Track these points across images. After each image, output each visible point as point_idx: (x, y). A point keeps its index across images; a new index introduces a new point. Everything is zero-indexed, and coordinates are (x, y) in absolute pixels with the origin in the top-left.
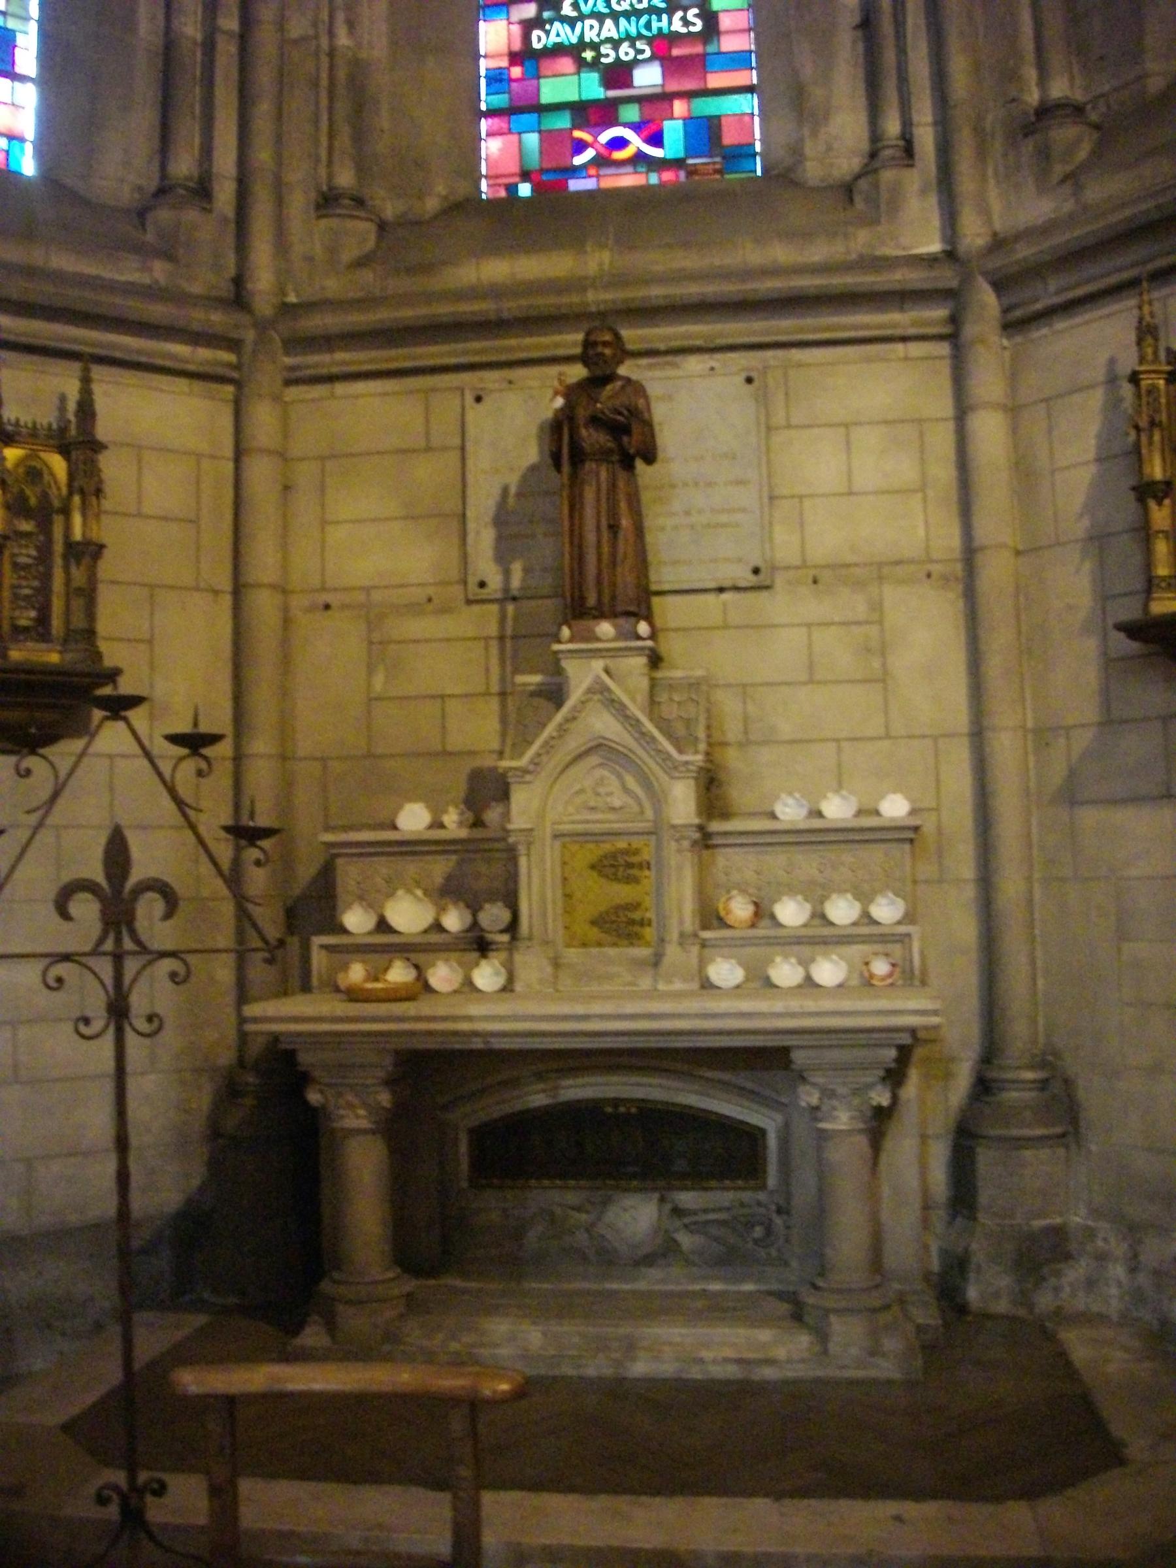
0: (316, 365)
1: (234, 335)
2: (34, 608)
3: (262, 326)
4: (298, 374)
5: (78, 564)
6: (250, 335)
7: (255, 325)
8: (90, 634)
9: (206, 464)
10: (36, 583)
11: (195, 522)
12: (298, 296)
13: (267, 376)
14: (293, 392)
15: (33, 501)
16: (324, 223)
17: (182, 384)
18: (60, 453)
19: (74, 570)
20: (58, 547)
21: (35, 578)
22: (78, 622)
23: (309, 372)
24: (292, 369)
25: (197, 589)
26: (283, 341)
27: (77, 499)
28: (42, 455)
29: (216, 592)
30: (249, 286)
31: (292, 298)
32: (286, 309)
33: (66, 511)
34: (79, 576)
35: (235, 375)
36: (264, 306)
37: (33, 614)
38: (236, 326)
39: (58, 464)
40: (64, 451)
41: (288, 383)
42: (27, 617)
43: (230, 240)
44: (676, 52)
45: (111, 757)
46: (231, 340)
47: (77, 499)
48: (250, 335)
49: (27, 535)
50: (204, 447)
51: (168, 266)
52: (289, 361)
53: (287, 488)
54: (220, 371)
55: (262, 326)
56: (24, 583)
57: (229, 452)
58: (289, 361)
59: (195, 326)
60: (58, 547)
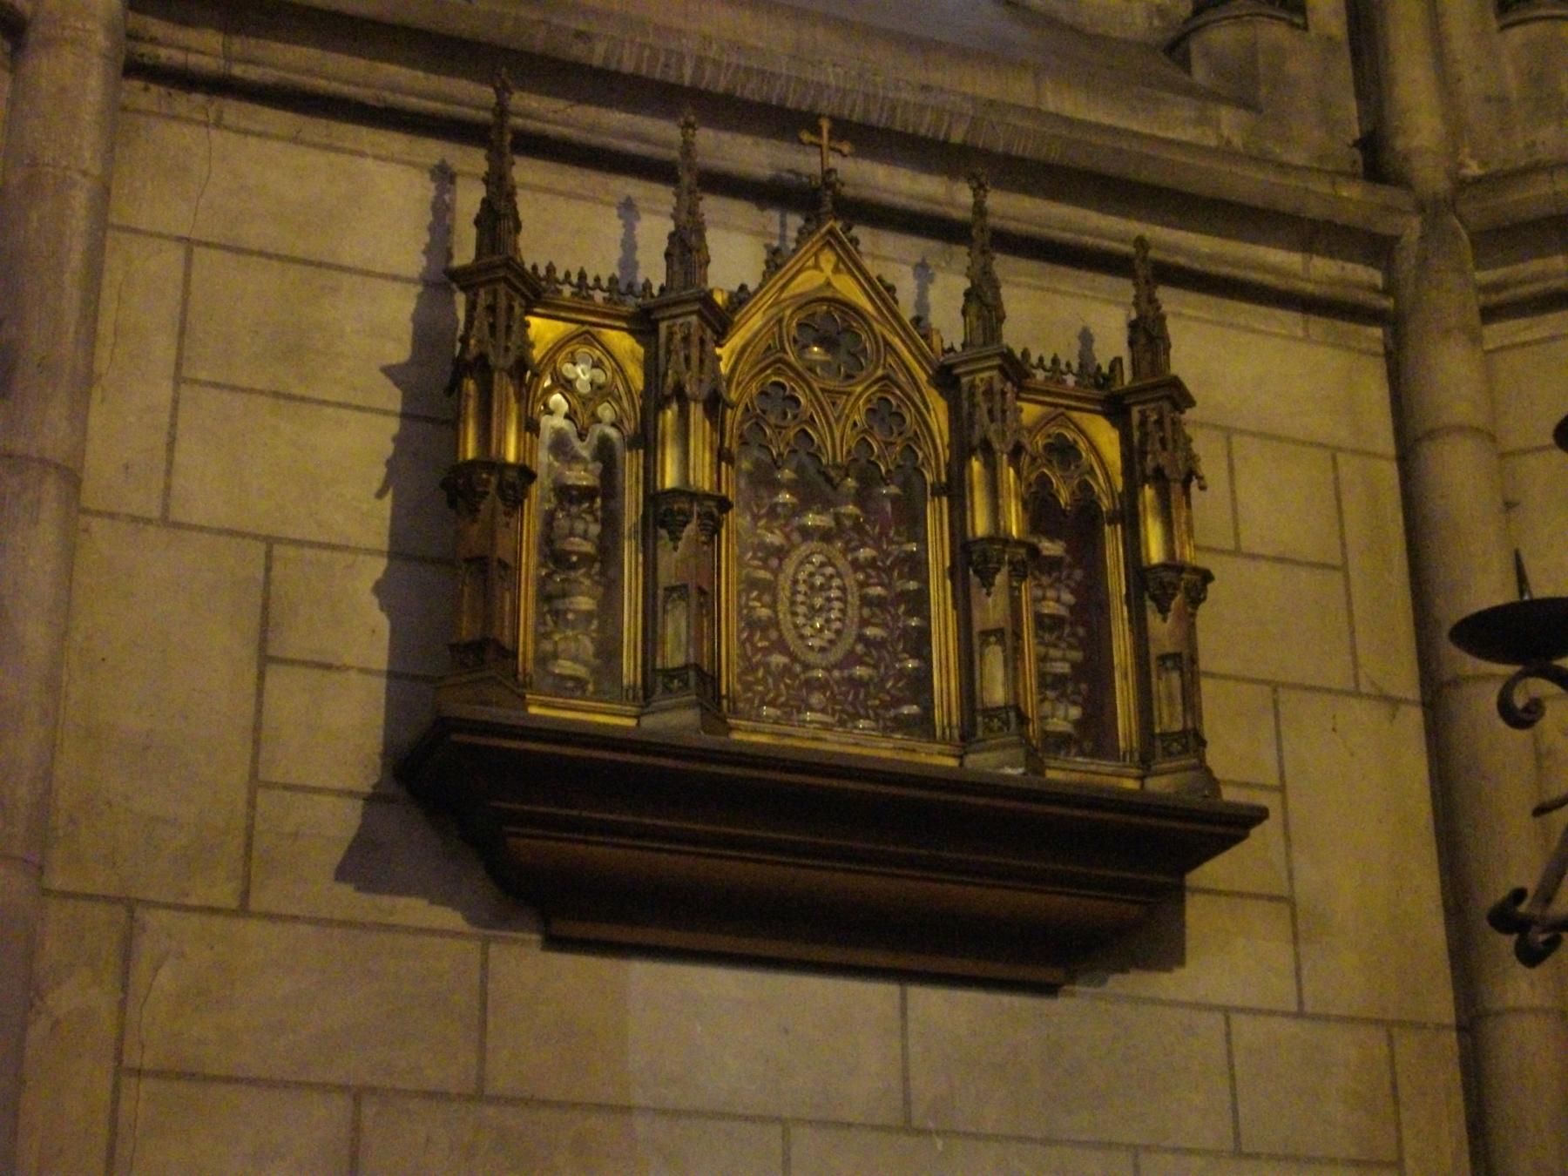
0: (1542, 276)
1: (1383, 227)
2: (1074, 703)
3: (1431, 210)
4: (1504, 296)
5: (1163, 610)
6: (1411, 229)
7: (1420, 208)
8: (1193, 740)
9: (1349, 467)
10: (1076, 655)
11: (1344, 568)
12: (1483, 164)
13: (1451, 292)
14: (1496, 333)
15: (1064, 497)
16: (1517, 35)
17: (1288, 321)
18: (1107, 415)
19: (1154, 620)
20: (1117, 583)
21: (1071, 647)
22: (1169, 719)
23: (1525, 290)
24: (1497, 287)
25: (1357, 694)
26: (1471, 234)
27: (1149, 493)
28: (1075, 415)
29: (1393, 702)
30: (1400, 144)
31: (1473, 169)
32: (1462, 185)
33: (1130, 521)
34: (1162, 629)
35: (1388, 303)
36: (1431, 176)
37: (1075, 712)
38: (1388, 209)
39: (1106, 438)
40: (1115, 409)
41: (1490, 314)
42: (1064, 717)
43: (1343, 70)
44: (470, 386)
45: (1227, 1011)
46: (1373, 238)
47: (1149, 493)
48: (1411, 229)
49: (1053, 564)
50: (1342, 435)
51: (1243, 114)
52: (1483, 277)
53: (1509, 505)
54: (1362, 296)
55: (1431, 210)
56: (1053, 653)
57: (1385, 442)
58: (1483, 277)
59: (1315, 210)
60: (1117, 583)
